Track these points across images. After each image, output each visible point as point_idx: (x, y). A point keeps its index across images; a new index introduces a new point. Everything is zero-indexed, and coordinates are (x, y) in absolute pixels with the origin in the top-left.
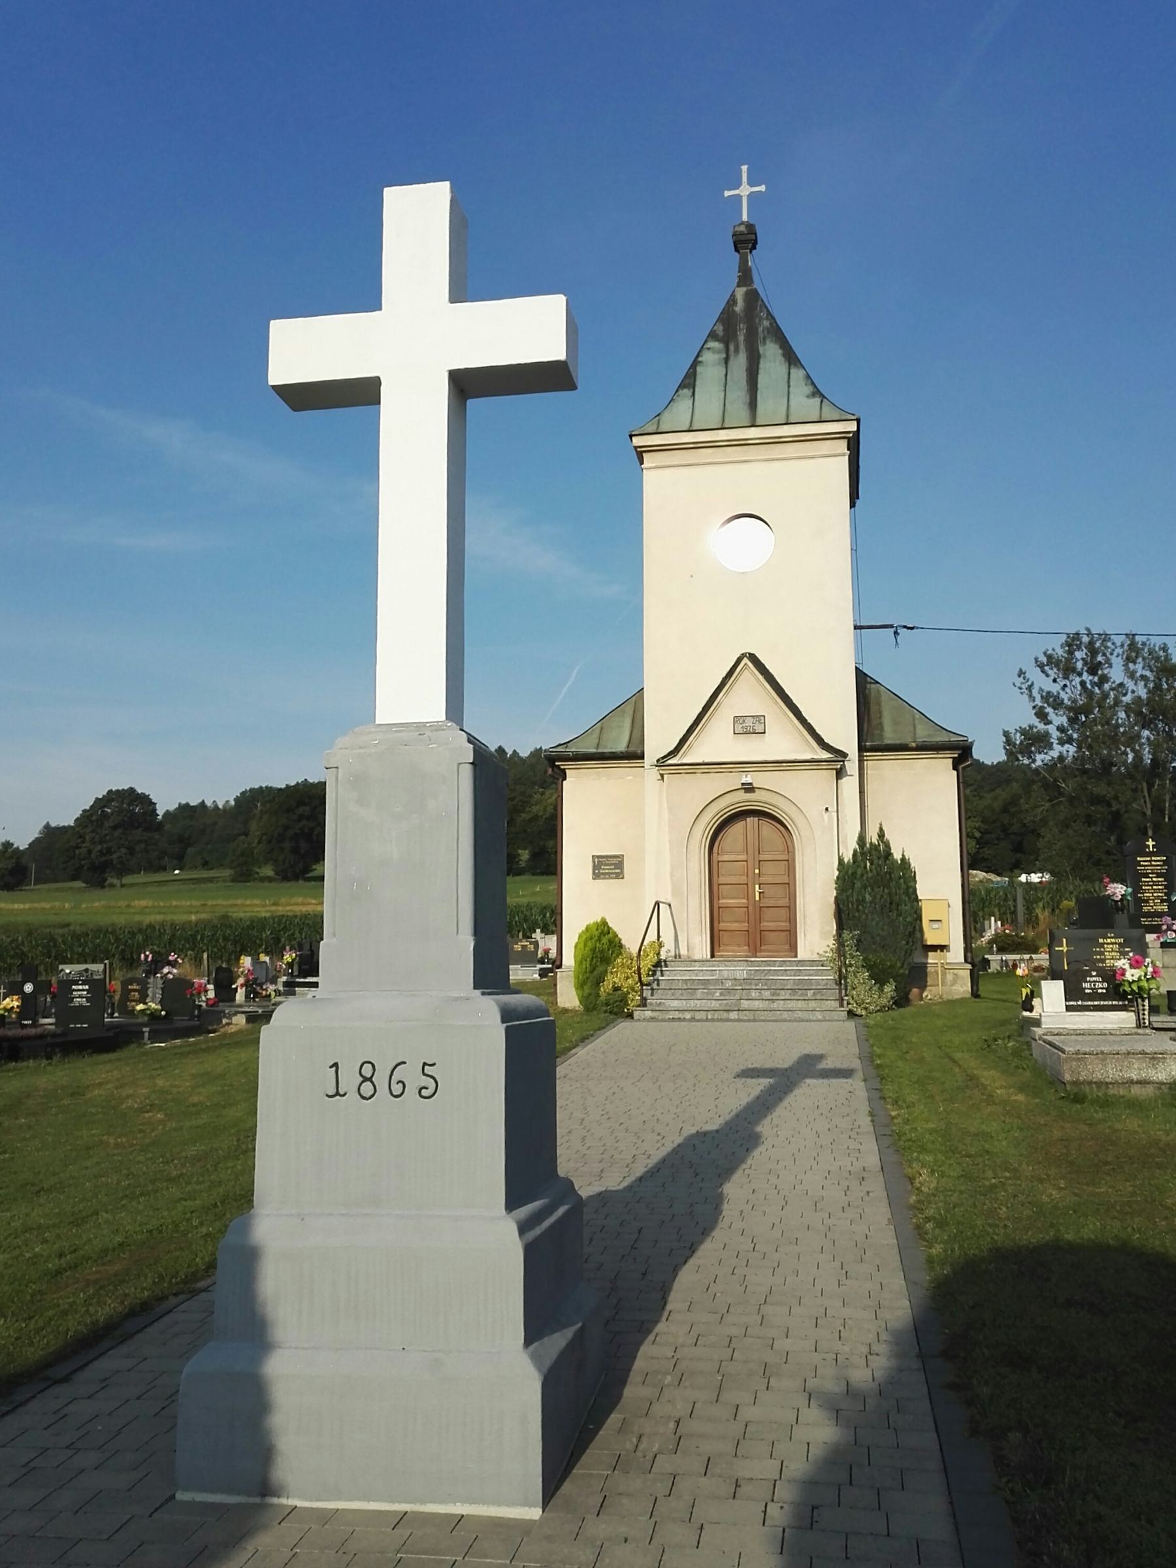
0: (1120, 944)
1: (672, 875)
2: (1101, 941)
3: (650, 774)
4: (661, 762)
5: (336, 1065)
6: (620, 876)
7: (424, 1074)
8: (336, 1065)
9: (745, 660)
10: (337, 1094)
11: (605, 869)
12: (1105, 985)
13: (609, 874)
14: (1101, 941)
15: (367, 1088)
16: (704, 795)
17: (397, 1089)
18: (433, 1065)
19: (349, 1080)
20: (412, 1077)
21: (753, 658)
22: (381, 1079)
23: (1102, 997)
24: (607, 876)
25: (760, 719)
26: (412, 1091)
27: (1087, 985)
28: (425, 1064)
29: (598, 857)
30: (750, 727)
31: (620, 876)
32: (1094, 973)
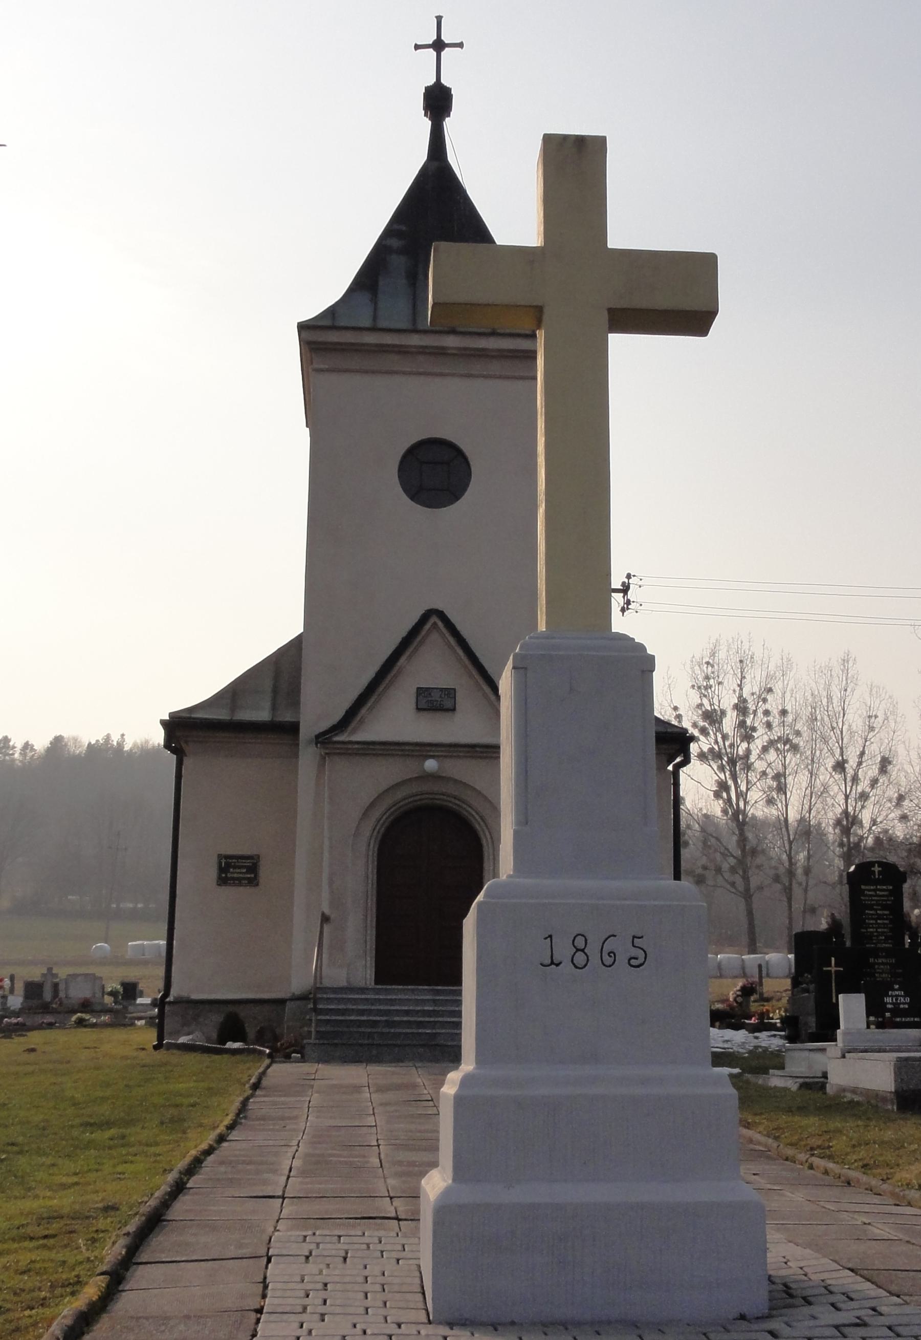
0: (890, 964)
1: (331, 882)
2: (871, 960)
3: (308, 756)
4: (323, 739)
5: (550, 936)
6: (253, 882)
7: (634, 946)
8: (550, 936)
9: (434, 619)
10: (552, 963)
11: (234, 873)
12: (908, 1000)
13: (237, 879)
14: (871, 960)
15: (580, 958)
16: (366, 787)
17: (608, 960)
18: (642, 937)
19: (563, 950)
20: (624, 950)
21: (441, 615)
22: (593, 950)
23: (904, 1013)
24: (238, 882)
25: (450, 693)
26: (622, 959)
27: (889, 1000)
28: (634, 937)
29: (227, 857)
30: (435, 702)
31: (253, 882)
32: (897, 987)
